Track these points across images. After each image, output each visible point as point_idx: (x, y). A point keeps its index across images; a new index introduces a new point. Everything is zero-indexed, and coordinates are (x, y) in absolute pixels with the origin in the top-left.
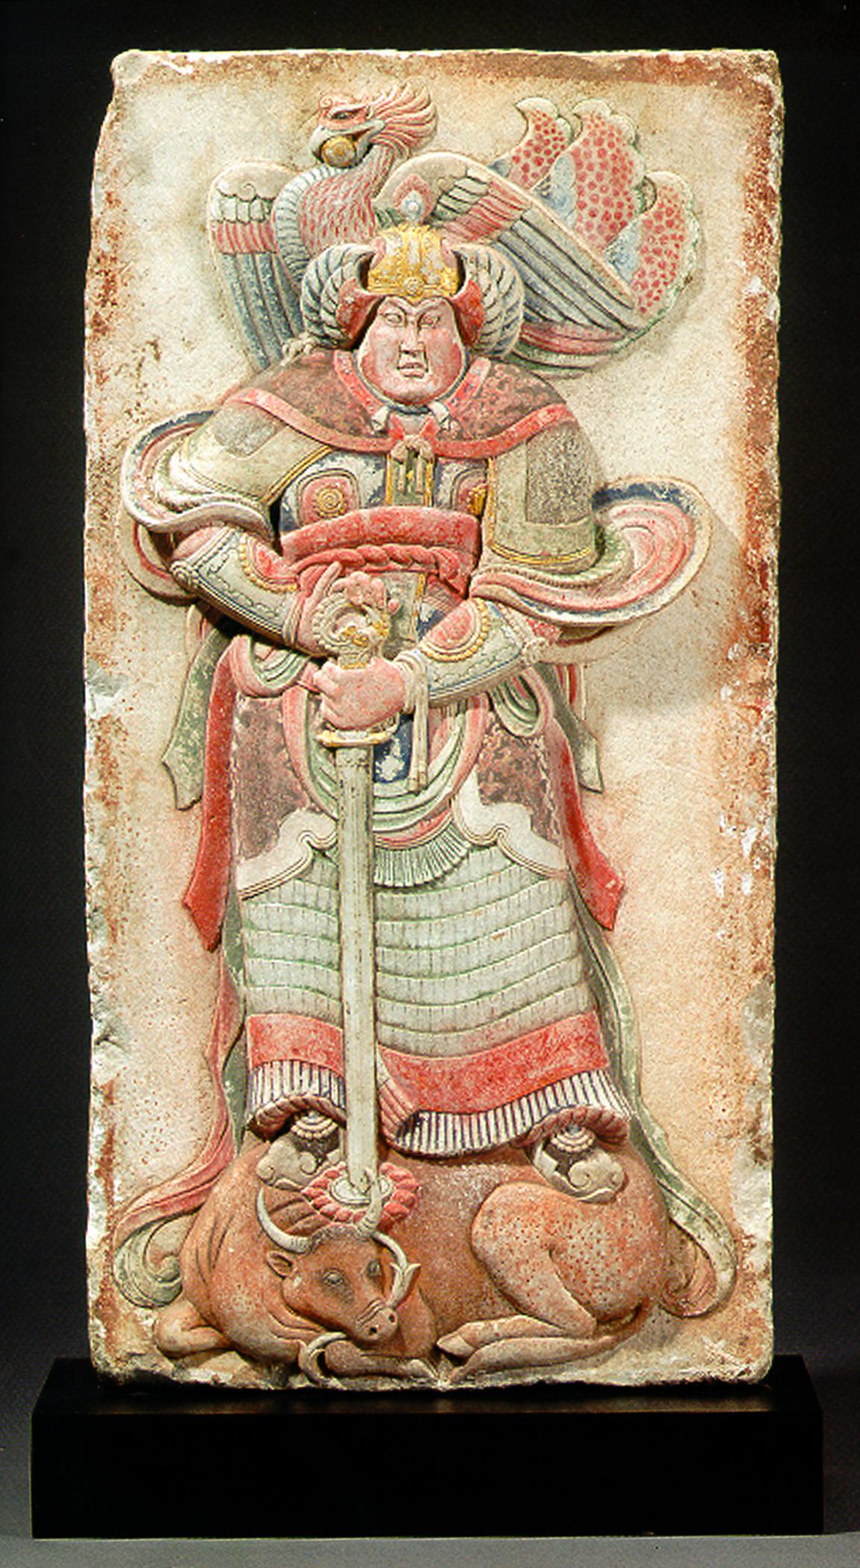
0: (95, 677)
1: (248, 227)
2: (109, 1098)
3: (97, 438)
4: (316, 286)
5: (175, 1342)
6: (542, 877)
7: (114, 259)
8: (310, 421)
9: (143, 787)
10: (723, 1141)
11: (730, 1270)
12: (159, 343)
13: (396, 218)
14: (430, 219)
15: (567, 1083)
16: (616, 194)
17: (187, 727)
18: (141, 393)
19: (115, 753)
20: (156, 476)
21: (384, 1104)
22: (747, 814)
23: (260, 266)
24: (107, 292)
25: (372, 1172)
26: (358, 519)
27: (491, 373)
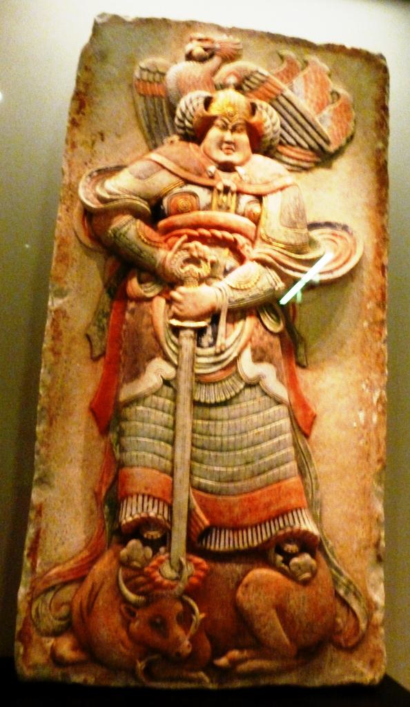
0: (55, 289)
2: (39, 513)
3: (68, 173)
5: (246, 70)
9: (76, 347)
13: (223, 86)
14: (238, 88)
15: (290, 515)
21: (192, 521)
22: (375, 383)
25: (183, 560)
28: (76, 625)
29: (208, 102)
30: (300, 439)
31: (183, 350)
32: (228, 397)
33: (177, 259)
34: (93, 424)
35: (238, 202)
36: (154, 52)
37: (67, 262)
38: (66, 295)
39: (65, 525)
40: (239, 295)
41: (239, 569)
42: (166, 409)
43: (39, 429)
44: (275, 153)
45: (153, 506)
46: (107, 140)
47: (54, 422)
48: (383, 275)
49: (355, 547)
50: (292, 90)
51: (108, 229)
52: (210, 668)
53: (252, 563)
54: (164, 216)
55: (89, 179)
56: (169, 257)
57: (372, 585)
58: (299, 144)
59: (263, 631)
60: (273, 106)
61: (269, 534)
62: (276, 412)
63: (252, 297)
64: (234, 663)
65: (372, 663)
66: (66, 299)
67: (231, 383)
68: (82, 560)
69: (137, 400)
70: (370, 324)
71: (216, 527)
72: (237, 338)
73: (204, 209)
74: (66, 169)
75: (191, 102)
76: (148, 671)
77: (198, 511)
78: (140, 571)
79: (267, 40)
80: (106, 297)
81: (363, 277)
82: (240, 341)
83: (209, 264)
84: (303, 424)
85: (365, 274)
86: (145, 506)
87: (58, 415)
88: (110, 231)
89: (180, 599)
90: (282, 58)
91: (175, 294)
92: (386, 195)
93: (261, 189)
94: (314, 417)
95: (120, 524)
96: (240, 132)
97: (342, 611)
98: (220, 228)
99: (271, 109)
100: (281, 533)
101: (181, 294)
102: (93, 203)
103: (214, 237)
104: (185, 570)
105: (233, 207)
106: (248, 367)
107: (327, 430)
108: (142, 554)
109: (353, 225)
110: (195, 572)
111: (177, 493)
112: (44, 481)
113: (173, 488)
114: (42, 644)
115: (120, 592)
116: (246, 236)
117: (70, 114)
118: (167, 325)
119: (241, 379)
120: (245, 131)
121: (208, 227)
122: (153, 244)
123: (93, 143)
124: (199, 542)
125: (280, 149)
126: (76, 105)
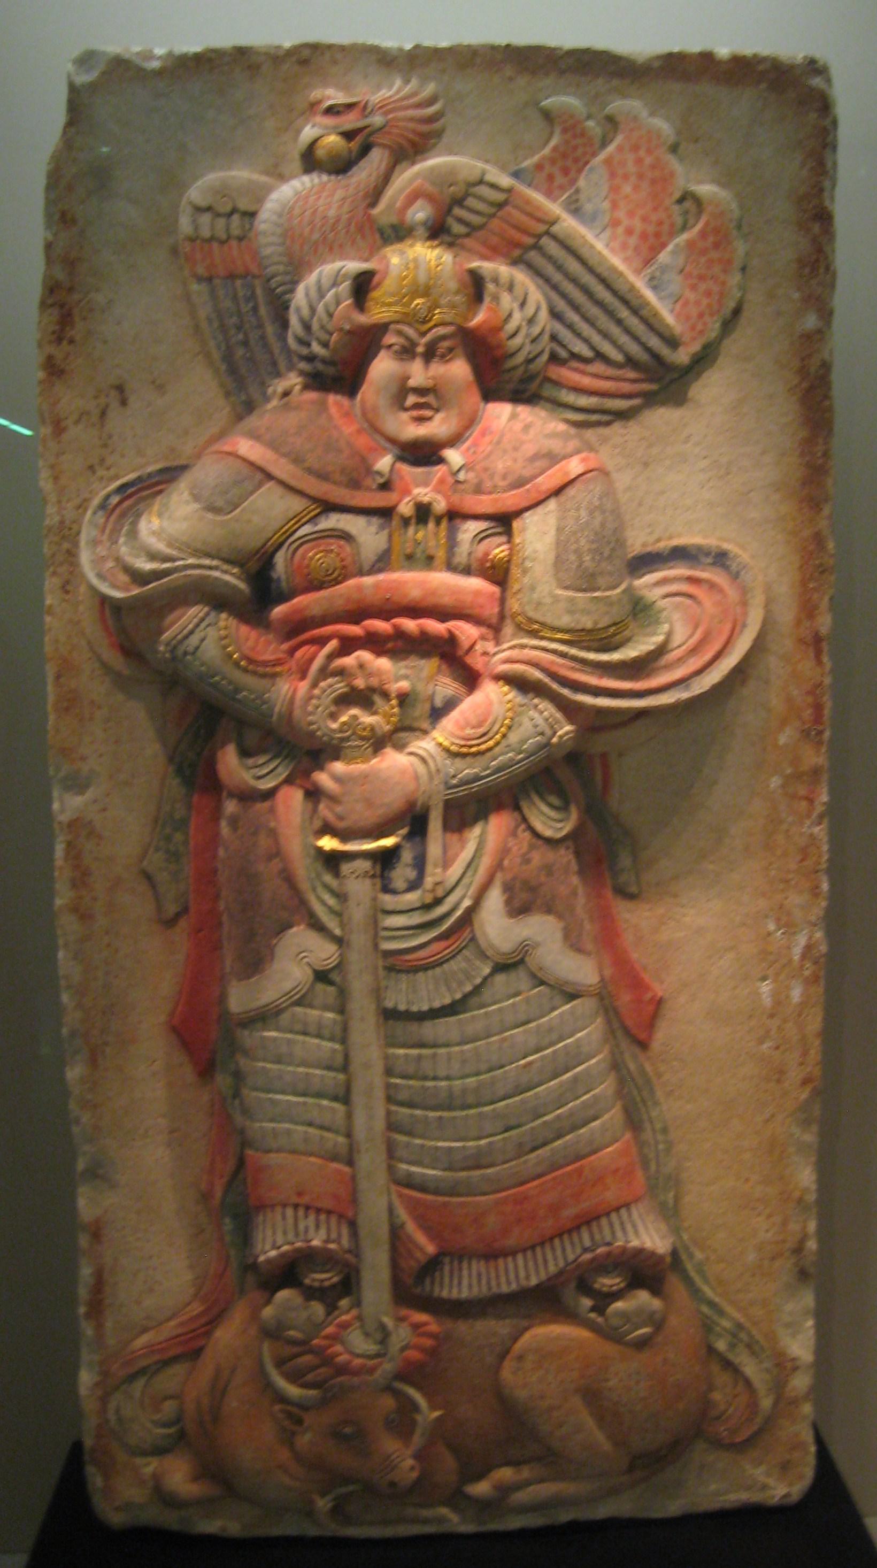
0: (62, 774)
1: (226, 247)
2: (96, 1233)
4: (305, 312)
6: (573, 997)
7: (71, 290)
13: (399, 233)
14: (437, 231)
16: (655, 209)
20: (122, 540)
23: (241, 294)
25: (388, 1321)
27: (513, 416)
29: (363, 286)
31: (352, 903)
32: (458, 996)
33: (319, 698)
35: (452, 543)
39: (152, 1262)
40: (468, 770)
41: (501, 1327)
42: (326, 1033)
43: (74, 1073)
44: (541, 385)
45: (317, 1227)
48: (819, 662)
49: (751, 1257)
50: (575, 210)
52: (457, 1498)
55: (100, 518)
56: (299, 694)
58: (600, 356)
63: (498, 770)
64: (504, 1490)
65: (785, 1467)
66: (90, 794)
68: (192, 1319)
69: (264, 1017)
72: (469, 865)
76: (337, 1511)
77: (411, 1227)
78: (303, 1345)
79: (508, 71)
80: (174, 783)
82: (476, 871)
83: (394, 702)
84: (632, 1015)
86: (301, 1227)
88: (162, 648)
89: (389, 1389)
90: (548, 116)
91: (323, 779)
92: (826, 454)
93: (509, 500)
94: (659, 1003)
96: (446, 357)
97: (722, 1378)
98: (414, 611)
99: (521, 276)
100: (588, 1256)
102: (114, 586)
103: (400, 634)
105: (441, 554)
106: (497, 927)
108: (304, 1314)
110: (415, 1340)
112: (97, 1173)
115: (269, 1385)
116: (477, 620)
117: (40, 345)
118: (312, 852)
119: (483, 956)
120: (459, 351)
121: (388, 611)
122: (261, 670)
123: (103, 414)
125: (558, 372)
126: (54, 315)
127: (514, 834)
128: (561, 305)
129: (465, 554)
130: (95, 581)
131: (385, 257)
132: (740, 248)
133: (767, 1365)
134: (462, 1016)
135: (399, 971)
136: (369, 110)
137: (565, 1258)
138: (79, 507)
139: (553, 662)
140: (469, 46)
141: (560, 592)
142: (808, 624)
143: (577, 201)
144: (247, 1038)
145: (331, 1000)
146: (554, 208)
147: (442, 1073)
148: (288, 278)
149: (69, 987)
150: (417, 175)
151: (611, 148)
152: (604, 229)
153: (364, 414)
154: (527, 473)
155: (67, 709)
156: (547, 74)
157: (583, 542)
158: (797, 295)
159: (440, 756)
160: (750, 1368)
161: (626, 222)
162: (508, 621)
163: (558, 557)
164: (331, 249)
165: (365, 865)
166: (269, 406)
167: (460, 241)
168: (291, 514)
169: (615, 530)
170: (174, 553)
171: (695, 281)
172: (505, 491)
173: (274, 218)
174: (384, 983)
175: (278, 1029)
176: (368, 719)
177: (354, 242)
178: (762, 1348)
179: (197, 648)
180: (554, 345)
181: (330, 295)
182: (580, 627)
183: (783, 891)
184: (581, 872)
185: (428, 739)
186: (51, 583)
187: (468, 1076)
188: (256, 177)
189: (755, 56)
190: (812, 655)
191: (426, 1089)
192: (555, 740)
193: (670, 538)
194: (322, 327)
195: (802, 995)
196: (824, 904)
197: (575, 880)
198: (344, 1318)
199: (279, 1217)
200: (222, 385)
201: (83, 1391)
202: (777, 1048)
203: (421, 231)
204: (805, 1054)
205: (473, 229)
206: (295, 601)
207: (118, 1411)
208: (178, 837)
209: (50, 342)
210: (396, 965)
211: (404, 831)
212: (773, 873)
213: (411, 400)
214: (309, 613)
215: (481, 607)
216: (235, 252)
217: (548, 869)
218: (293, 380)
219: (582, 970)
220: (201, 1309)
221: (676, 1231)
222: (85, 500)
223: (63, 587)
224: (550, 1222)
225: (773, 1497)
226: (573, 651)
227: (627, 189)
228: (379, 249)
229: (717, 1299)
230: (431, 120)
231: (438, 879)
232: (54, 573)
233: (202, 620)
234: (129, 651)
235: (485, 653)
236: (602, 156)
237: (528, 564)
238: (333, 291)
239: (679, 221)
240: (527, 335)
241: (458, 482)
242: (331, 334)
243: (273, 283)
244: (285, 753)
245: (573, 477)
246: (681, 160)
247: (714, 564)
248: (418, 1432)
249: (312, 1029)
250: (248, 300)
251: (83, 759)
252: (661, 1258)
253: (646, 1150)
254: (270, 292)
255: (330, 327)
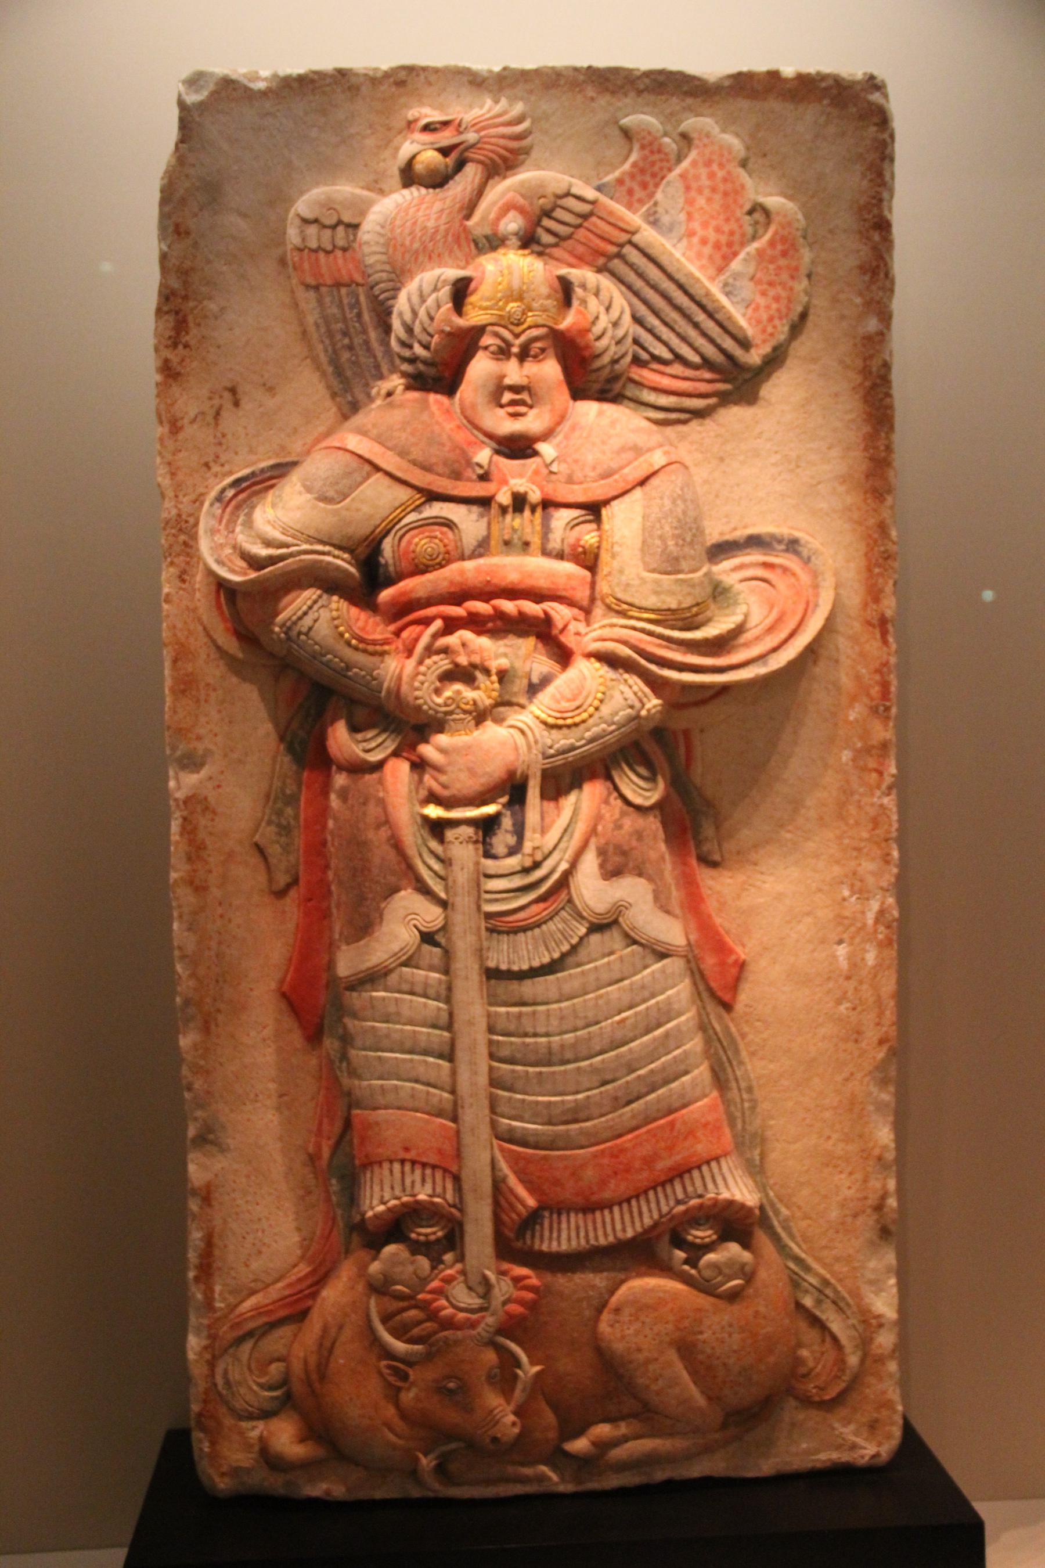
0: (179, 753)
1: (331, 257)
2: (207, 1196)
3: (171, 494)
4: (408, 316)
6: (662, 956)
7: (186, 298)
8: (404, 464)
10: (849, 1220)
11: (859, 1353)
12: (240, 390)
13: (494, 243)
14: (528, 241)
16: (727, 220)
17: (279, 805)
18: (220, 444)
19: (202, 835)
20: (238, 529)
21: (503, 1202)
22: (871, 880)
23: (346, 301)
24: (178, 334)
25: (491, 1276)
26: (462, 572)
27: (600, 413)
28: (301, 1397)
29: (461, 292)
30: (713, 1009)
31: (456, 868)
32: (556, 955)
34: (289, 1022)
35: (546, 530)
36: (328, 168)
37: (194, 693)
38: (202, 765)
40: (562, 740)
41: (599, 1280)
43: (186, 1041)
45: (424, 1181)
46: (247, 405)
47: (213, 1027)
48: (885, 642)
49: (834, 1214)
50: (655, 223)
51: (272, 623)
52: (558, 1457)
53: (625, 1269)
54: (390, 581)
55: (217, 510)
56: (406, 671)
57: (871, 1282)
58: (679, 358)
59: (654, 1387)
60: (613, 274)
61: (656, 1216)
62: (657, 975)
63: (591, 741)
64: (603, 1446)
65: (873, 1426)
66: (204, 773)
67: (560, 926)
68: (300, 1280)
69: (374, 977)
70: (858, 754)
71: (552, 1207)
72: (566, 830)
73: (472, 556)
74: (166, 482)
75: (423, 299)
76: (441, 1469)
77: (513, 1181)
78: (408, 1299)
79: (590, 92)
81: (837, 649)
82: (571, 837)
83: (494, 678)
84: (718, 979)
85: (842, 642)
86: (408, 1182)
87: (219, 1011)
88: (277, 629)
90: (627, 134)
91: (427, 750)
92: (889, 449)
93: (596, 491)
94: (742, 966)
95: (363, 1214)
97: (811, 1335)
98: (512, 593)
99: (606, 282)
100: (681, 1208)
101: (442, 750)
102: (232, 571)
103: (500, 615)
104: (496, 1291)
105: (536, 541)
106: (592, 890)
107: (774, 987)
108: (410, 1269)
109: (811, 539)
111: (466, 1152)
112: (208, 1139)
113: (459, 1143)
114: (241, 1433)
115: (372, 1330)
116: (570, 603)
117: (157, 350)
118: (419, 820)
120: (551, 352)
121: (487, 594)
122: (370, 648)
123: (218, 414)
124: (518, 1239)
127: (606, 802)
128: (643, 310)
129: (559, 540)
130: (215, 567)
131: (481, 265)
132: (806, 255)
133: (853, 1321)
134: (559, 975)
135: (499, 933)
136: (463, 126)
137: (660, 1210)
138: (194, 502)
139: (640, 640)
140: (553, 68)
141: (646, 574)
142: (875, 607)
143: (655, 212)
144: (356, 999)
145: (436, 961)
146: (634, 219)
147: (541, 1030)
148: (390, 285)
149: (183, 957)
150: (509, 189)
151: (685, 164)
152: (680, 240)
153: (463, 413)
154: (614, 465)
155: (183, 692)
156: (626, 95)
157: (667, 528)
158: (858, 300)
159: (539, 730)
160: (836, 1326)
161: (700, 232)
162: (599, 603)
163: (644, 542)
164: (430, 257)
165: (468, 831)
166: (374, 406)
167: (548, 251)
168: (397, 504)
169: (695, 519)
170: (290, 540)
171: (765, 287)
172: (596, 481)
173: (378, 229)
174: (485, 944)
175: (385, 990)
176: (469, 694)
177: (451, 251)
178: (848, 1305)
179: (310, 629)
180: (636, 348)
181: (430, 301)
182: (665, 607)
183: (856, 858)
184: (667, 841)
185: (526, 712)
186: (168, 574)
187: (566, 1032)
188: (358, 191)
189: (818, 73)
190: (878, 636)
191: (526, 1045)
192: (644, 713)
193: (745, 527)
194: (425, 330)
195: (877, 957)
196: (895, 870)
197: (663, 847)
198: (449, 1272)
199: (386, 1172)
200: (329, 387)
201: (191, 1356)
202: (854, 1009)
203: (514, 241)
204: (881, 1014)
205: (561, 238)
206: (402, 584)
207: (226, 1372)
208: (289, 811)
209: (167, 347)
210: (498, 926)
211: (504, 800)
212: (846, 841)
213: (507, 397)
214: (414, 595)
215: (574, 589)
216: (340, 261)
217: (639, 835)
218: (396, 382)
219: (672, 932)
220: (309, 1269)
221: (762, 1188)
222: (202, 494)
223: (180, 577)
224: (645, 1174)
225: (863, 1457)
226: (659, 630)
227: (701, 201)
228: (473, 259)
229: (803, 1255)
230: (519, 137)
231: (537, 844)
232: (172, 564)
233: (315, 602)
234: (246, 637)
235: (578, 634)
236: (678, 171)
237: (617, 548)
238: (434, 296)
239: (749, 230)
240: (613, 338)
241: (551, 473)
242: (432, 336)
243: (376, 291)
244: (392, 727)
245: (657, 467)
246: (750, 176)
247: (787, 550)
248: (519, 1386)
249: (419, 989)
250: (352, 307)
251: (199, 738)
252: (750, 1210)
253: (732, 1108)
254: (374, 299)
255: (430, 330)
